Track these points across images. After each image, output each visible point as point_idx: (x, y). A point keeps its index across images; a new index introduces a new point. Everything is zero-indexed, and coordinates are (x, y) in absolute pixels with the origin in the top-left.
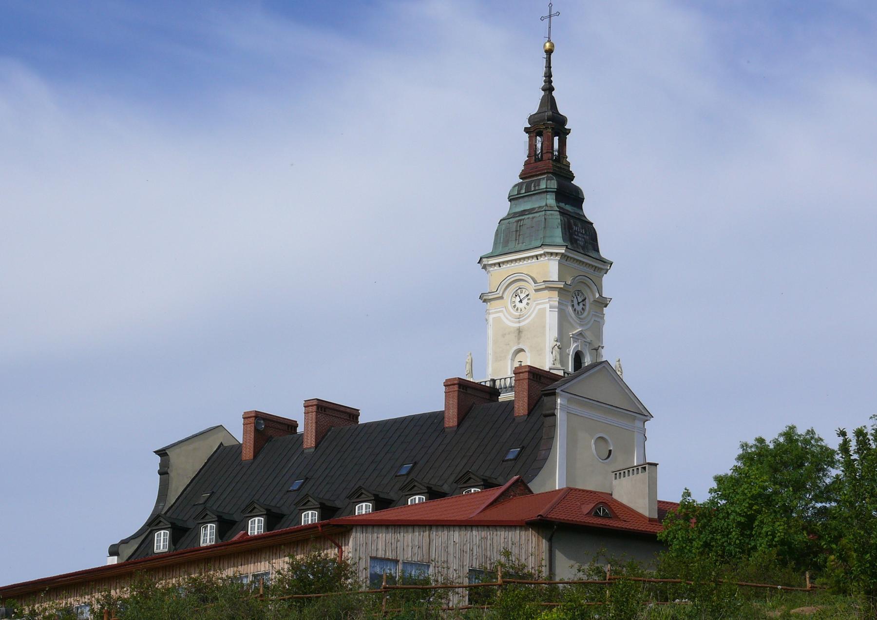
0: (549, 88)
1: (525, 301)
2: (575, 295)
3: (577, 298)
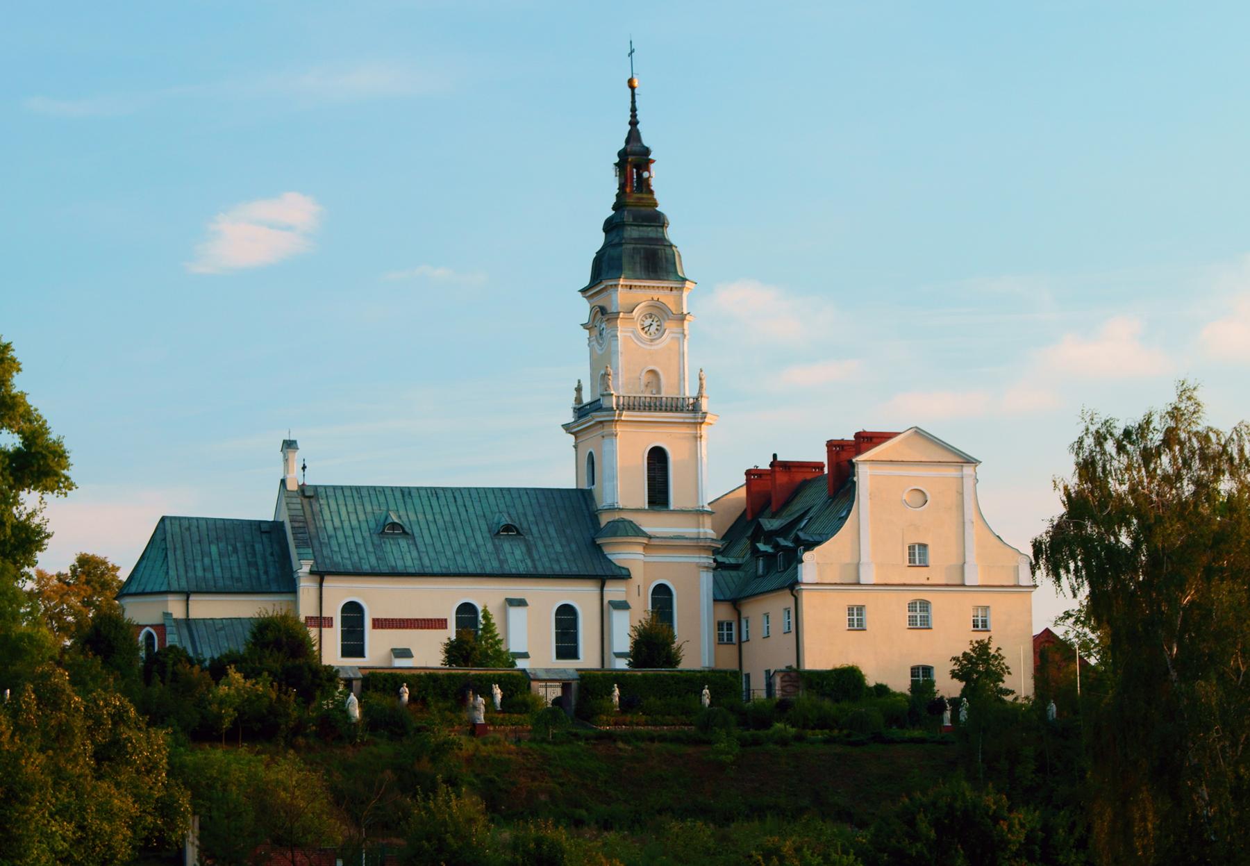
0: (634, 123)
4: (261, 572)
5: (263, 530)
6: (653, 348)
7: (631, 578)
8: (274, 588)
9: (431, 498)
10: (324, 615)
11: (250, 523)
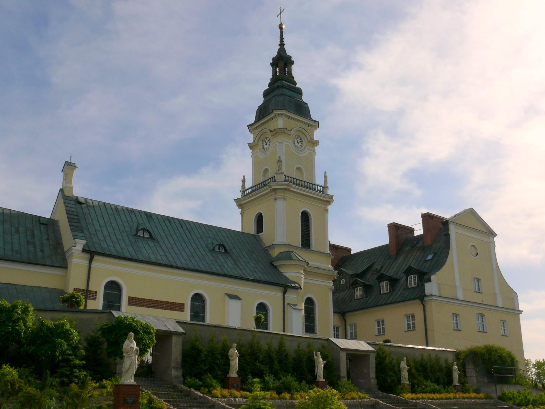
0: (282, 44)
1: (268, 144)
2: (296, 138)
3: (297, 140)
4: (38, 250)
5: (41, 222)
6: (299, 155)
8: (48, 262)
9: (165, 221)
10: (90, 289)
11: (32, 216)
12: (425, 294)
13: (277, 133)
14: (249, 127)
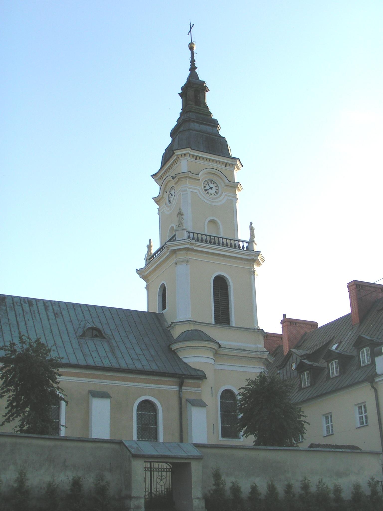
0: (193, 68)
7: (206, 378)
12: (376, 373)
13: (179, 179)
14: (153, 177)
